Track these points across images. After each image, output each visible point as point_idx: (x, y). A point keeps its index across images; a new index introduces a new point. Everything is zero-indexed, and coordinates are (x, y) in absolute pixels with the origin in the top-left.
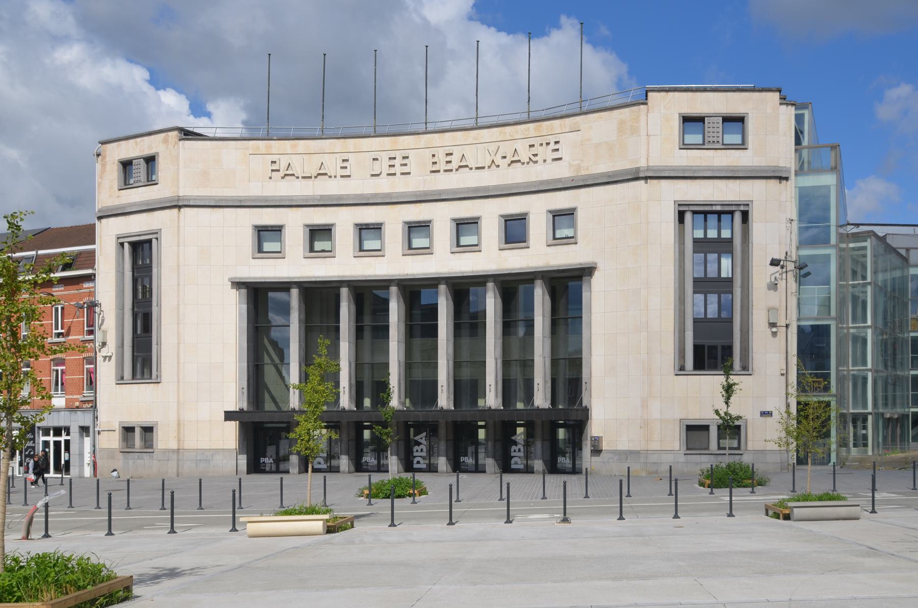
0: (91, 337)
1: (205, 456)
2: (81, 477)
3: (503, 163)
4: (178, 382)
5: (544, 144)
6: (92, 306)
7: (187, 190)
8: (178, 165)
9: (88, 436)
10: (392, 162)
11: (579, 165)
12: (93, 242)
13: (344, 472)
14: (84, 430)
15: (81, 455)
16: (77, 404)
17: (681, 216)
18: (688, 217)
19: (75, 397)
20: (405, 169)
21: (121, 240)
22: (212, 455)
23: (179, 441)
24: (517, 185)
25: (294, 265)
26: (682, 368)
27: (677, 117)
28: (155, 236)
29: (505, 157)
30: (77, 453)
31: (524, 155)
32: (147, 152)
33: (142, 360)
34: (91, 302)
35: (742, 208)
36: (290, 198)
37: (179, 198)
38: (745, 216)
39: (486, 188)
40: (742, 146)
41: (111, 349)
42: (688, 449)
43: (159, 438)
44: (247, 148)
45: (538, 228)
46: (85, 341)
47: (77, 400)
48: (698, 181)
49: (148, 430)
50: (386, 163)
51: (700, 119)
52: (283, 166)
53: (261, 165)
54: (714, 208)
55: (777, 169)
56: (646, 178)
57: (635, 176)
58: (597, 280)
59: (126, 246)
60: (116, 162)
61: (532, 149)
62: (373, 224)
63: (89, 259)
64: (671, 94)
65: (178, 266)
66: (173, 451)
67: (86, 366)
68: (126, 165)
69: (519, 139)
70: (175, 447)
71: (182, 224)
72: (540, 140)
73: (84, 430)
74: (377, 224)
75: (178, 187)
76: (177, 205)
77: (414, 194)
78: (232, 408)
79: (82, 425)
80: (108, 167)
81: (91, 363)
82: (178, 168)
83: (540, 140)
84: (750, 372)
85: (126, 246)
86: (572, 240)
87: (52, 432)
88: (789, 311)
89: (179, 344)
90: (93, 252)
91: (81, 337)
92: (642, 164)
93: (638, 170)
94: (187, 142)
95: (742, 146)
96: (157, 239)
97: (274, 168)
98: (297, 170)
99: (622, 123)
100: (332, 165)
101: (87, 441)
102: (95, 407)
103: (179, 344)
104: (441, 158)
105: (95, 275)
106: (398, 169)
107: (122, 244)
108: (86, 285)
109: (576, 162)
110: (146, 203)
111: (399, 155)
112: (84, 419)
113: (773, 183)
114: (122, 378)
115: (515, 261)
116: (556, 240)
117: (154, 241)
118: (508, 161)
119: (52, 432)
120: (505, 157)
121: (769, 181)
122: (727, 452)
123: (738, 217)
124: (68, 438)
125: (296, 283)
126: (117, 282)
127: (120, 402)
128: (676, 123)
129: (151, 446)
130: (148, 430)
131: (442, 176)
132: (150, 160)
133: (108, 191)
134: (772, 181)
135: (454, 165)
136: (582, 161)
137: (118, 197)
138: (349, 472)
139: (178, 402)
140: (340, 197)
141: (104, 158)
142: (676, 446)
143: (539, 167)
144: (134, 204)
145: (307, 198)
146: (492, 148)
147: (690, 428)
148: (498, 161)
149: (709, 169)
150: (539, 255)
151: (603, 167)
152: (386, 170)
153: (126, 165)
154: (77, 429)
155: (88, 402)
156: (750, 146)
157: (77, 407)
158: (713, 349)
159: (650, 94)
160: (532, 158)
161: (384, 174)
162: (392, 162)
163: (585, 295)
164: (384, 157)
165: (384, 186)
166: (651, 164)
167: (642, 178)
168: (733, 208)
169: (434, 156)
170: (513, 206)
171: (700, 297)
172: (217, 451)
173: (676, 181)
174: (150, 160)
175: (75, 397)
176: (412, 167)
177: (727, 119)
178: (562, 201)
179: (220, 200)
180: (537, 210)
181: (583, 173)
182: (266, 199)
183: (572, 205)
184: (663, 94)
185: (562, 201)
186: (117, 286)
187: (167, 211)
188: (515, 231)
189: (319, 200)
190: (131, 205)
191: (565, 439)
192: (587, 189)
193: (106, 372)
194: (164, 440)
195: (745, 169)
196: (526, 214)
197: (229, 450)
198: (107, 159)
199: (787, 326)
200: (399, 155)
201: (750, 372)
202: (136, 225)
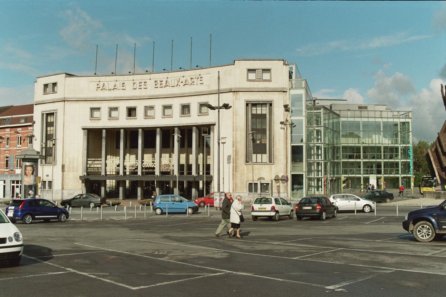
3: (182, 85)
5: (197, 78)
7: (68, 96)
10: (140, 84)
12: (33, 113)
17: (247, 105)
21: (43, 113)
25: (104, 122)
28: (56, 111)
29: (182, 83)
32: (54, 82)
35: (270, 102)
38: (271, 105)
45: (140, 112)
50: (138, 84)
53: (94, 86)
64: (240, 61)
68: (46, 86)
78: (81, 175)
86: (207, 114)
90: (32, 117)
97: (98, 87)
106: (143, 86)
107: (43, 114)
108: (30, 128)
115: (185, 121)
116: (146, 116)
117: (55, 113)
124: (13, 185)
132: (55, 84)
133: (39, 95)
135: (164, 85)
152: (138, 87)
153: (46, 86)
159: (235, 61)
160: (192, 83)
162: (140, 84)
165: (138, 93)
166: (236, 87)
174: (55, 84)
176: (148, 86)
188: (131, 112)
202: (48, 108)
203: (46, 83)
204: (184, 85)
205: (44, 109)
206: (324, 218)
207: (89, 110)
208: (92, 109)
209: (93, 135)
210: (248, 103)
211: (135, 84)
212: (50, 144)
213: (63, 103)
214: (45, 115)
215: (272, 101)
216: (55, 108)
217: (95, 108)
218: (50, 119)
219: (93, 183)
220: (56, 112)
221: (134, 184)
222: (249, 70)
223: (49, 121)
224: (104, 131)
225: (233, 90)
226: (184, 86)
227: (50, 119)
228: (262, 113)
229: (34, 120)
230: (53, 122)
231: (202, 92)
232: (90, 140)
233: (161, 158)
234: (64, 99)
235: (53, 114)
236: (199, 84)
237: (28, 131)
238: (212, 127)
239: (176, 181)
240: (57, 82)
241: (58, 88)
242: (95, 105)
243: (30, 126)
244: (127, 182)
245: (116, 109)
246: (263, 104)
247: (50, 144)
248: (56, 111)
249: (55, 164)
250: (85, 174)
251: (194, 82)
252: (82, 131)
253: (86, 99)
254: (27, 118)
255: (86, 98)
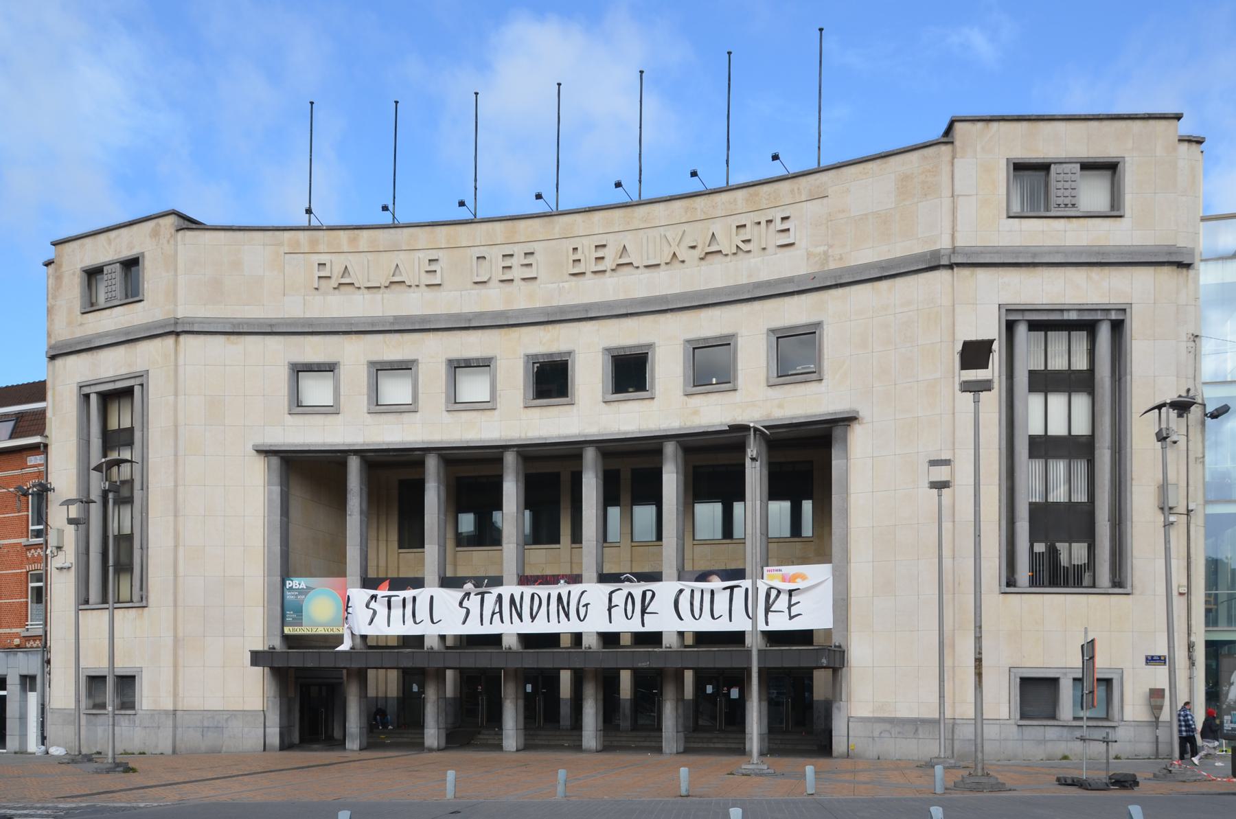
0: (40, 540)
1: (215, 721)
2: (22, 752)
4: (175, 606)
5: (763, 224)
6: (44, 491)
7: (186, 310)
8: (176, 270)
9: (33, 689)
10: (508, 263)
11: (825, 253)
12: (43, 399)
13: (431, 750)
14: (28, 682)
15: (23, 718)
16: (17, 641)
18: (1021, 331)
19: (14, 630)
20: (528, 273)
21: (86, 390)
22: (227, 720)
23: (175, 695)
24: (716, 291)
25: (353, 429)
26: (1011, 582)
27: (1003, 164)
28: (138, 381)
29: (693, 247)
30: (17, 715)
31: (724, 244)
32: (126, 254)
33: (116, 566)
34: (40, 484)
35: (1113, 316)
36: (348, 321)
37: (176, 321)
38: (1118, 327)
39: (664, 299)
40: (1115, 211)
41: (68, 557)
42: (1023, 717)
43: (146, 692)
44: (281, 244)
46: (29, 547)
47: (17, 635)
48: (1039, 270)
49: (127, 682)
51: (1044, 167)
52: (337, 270)
54: (1066, 316)
55: (1172, 249)
56: (951, 266)
57: (933, 264)
58: (858, 438)
59: (94, 398)
60: (78, 272)
61: (742, 230)
62: (477, 359)
63: (35, 423)
64: (995, 125)
65: (176, 426)
66: (166, 712)
67: (31, 585)
68: (93, 274)
69: (720, 219)
70: (170, 707)
71: (181, 361)
72: (756, 217)
73: (28, 682)
74: (484, 359)
75: (176, 305)
76: (175, 331)
77: (543, 310)
78: (259, 647)
79: (25, 673)
80: (66, 280)
81: (40, 580)
82: (176, 275)
83: (756, 217)
84: (1128, 590)
85: (94, 398)
86: (814, 376)
87: (755, 476)
88: (1191, 489)
89: (176, 547)
90: (42, 413)
91: (23, 541)
92: (944, 243)
93: (936, 254)
94: (189, 233)
95: (1115, 211)
96: (142, 385)
98: (356, 277)
99: (905, 179)
100: (412, 267)
101: (33, 698)
102: (45, 648)
103: (176, 547)
104: (588, 254)
105: (46, 446)
106: (517, 273)
107: (87, 396)
108: (34, 460)
109: (821, 249)
110: (127, 331)
111: (518, 250)
112: (29, 664)
113: (1166, 273)
114: (87, 602)
115: (712, 413)
117: (137, 390)
118: (698, 253)
119: (755, 476)
120: (693, 247)
121: (1159, 269)
122: (1084, 723)
123: (1104, 334)
125: (356, 452)
126: (79, 454)
127: (79, 637)
128: (1001, 173)
129: (132, 706)
130: (127, 682)
131: (589, 282)
132: (131, 265)
134: (1166, 269)
135: (608, 264)
136: (831, 246)
137: (81, 324)
138: (439, 750)
139: (175, 637)
140: (424, 318)
141: (60, 266)
142: (1004, 713)
143: (754, 261)
144: (107, 334)
145: (374, 320)
146: (671, 234)
147: (1024, 681)
148: (683, 253)
149: (1057, 250)
150: (757, 401)
151: (868, 255)
154: (17, 680)
155: (34, 638)
156: (1128, 211)
157: (18, 647)
158: (1062, 544)
159: (958, 126)
160: (742, 245)
161: (494, 282)
162: (508, 263)
163: (836, 463)
164: (495, 254)
165: (494, 300)
166: (960, 242)
167: (944, 266)
168: (1099, 316)
169: (575, 249)
170: (709, 324)
171: (1038, 465)
172: (233, 714)
173: (1001, 270)
174: (131, 265)
175: (14, 630)
177: (1088, 166)
178: (794, 312)
179: (239, 324)
180: (751, 330)
181: (833, 265)
182: (309, 322)
183: (813, 319)
184: (980, 125)
185: (794, 312)
186: (79, 460)
187: (157, 342)
189: (392, 324)
190: (99, 336)
191: (454, 699)
192: (840, 291)
193: (62, 589)
194: (149, 697)
195: (1120, 250)
196: (733, 336)
197: (253, 713)
198: (64, 269)
199: (1189, 512)
200: (518, 250)
201: (1128, 590)
202: (110, 367)
203: (92, 261)
204: (702, 259)
205: (88, 376)
206: (939, 769)
207: (283, 374)
208: (299, 369)
209: (309, 475)
210: (1011, 317)
211: (485, 264)
212: (122, 520)
213: (170, 340)
214: (94, 399)
215: (1124, 310)
216: (138, 368)
217: (311, 364)
218: (121, 418)
219: (311, 690)
220: (142, 385)
221: (650, 684)
222: (1020, 167)
223: (113, 425)
224: (354, 465)
225: (944, 261)
226: (703, 262)
227: (121, 418)
228: (717, 508)
229: (258, 670)
230: (131, 430)
231: (790, 280)
232: (295, 513)
233: (568, 583)
234: (176, 323)
235: (128, 393)
236: (771, 249)
237: (24, 471)
238: (837, 432)
239: (749, 670)
240: (143, 254)
241: (152, 277)
242: (313, 350)
243: (34, 449)
244: (626, 678)
245: (404, 367)
246: (1083, 325)
247: (122, 520)
248: (138, 381)
249: (144, 604)
250: (277, 643)
251: (749, 241)
252: (260, 464)
253: (271, 326)
254: (19, 417)
255: (274, 322)
